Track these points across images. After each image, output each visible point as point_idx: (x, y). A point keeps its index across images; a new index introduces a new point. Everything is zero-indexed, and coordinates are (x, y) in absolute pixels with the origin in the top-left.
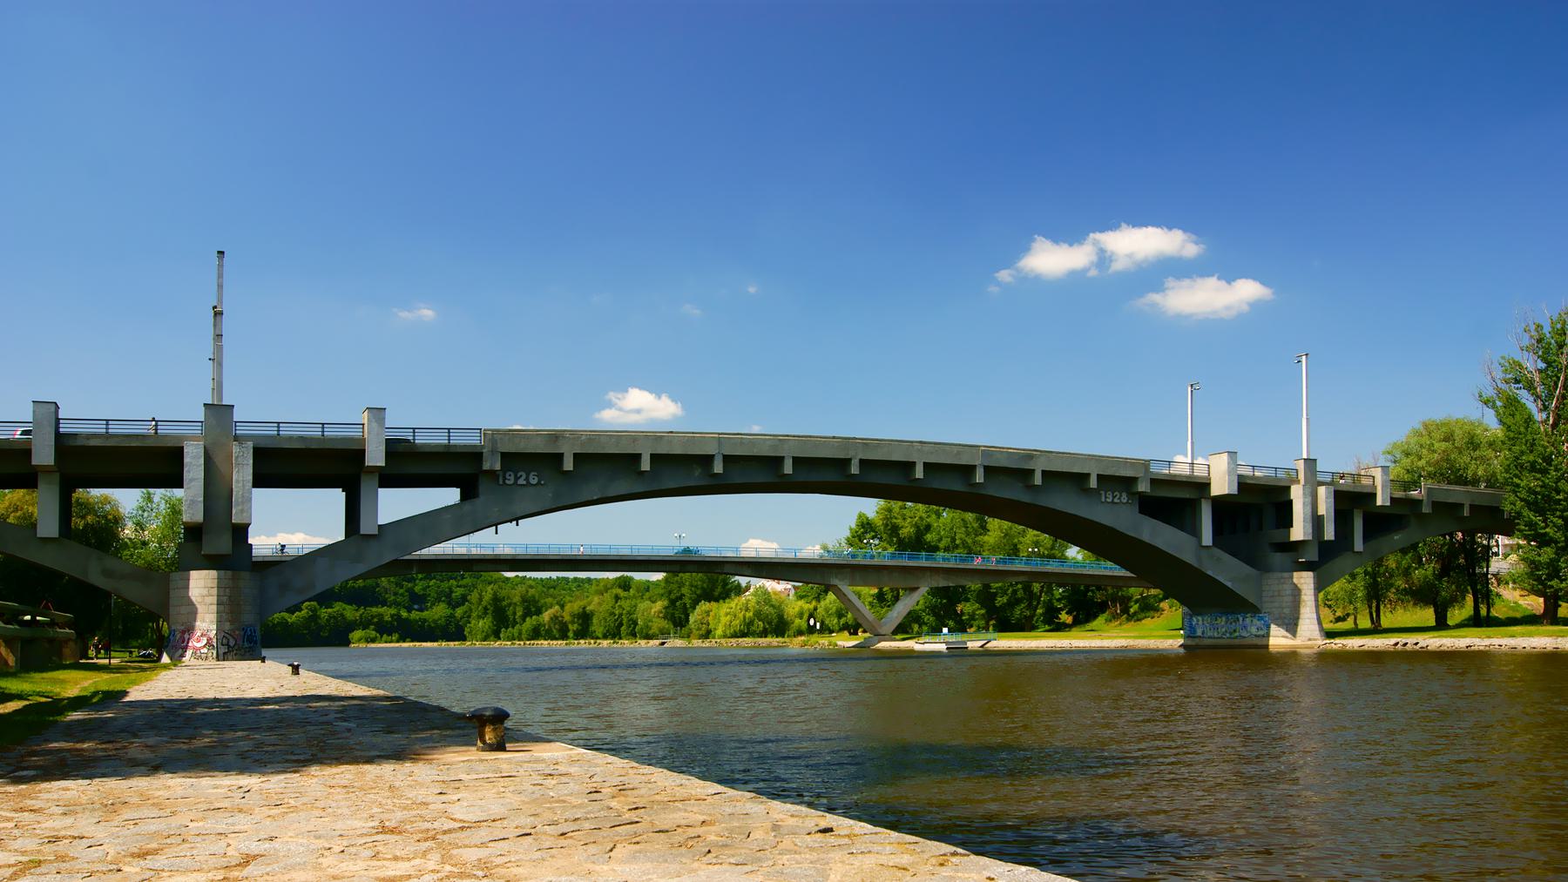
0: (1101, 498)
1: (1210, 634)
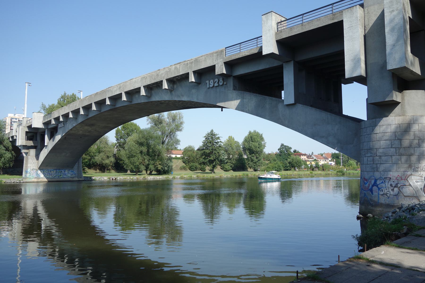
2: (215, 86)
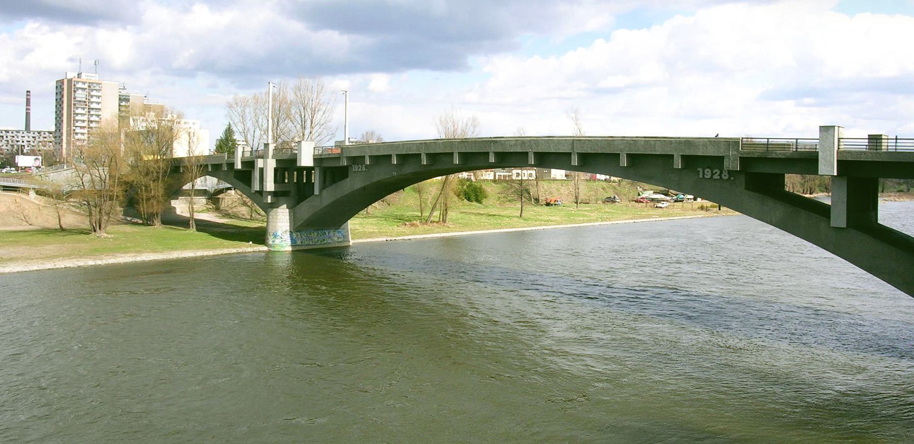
0: (699, 175)
2: (714, 178)
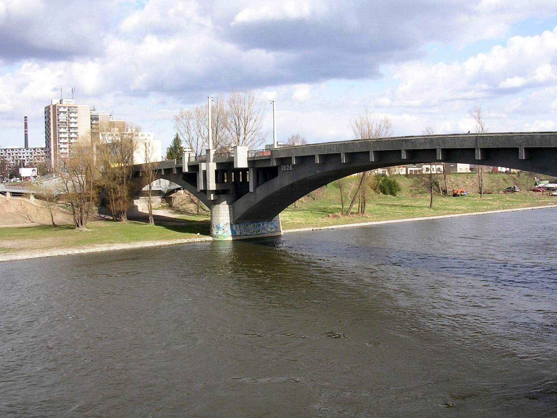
1: (245, 233)
